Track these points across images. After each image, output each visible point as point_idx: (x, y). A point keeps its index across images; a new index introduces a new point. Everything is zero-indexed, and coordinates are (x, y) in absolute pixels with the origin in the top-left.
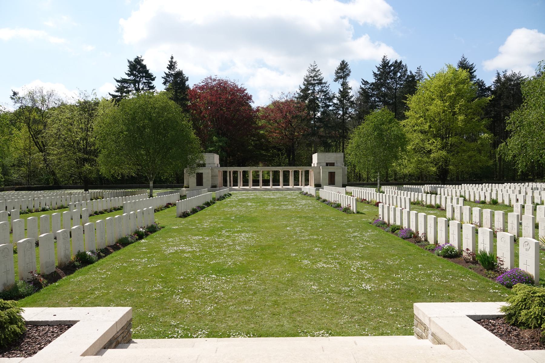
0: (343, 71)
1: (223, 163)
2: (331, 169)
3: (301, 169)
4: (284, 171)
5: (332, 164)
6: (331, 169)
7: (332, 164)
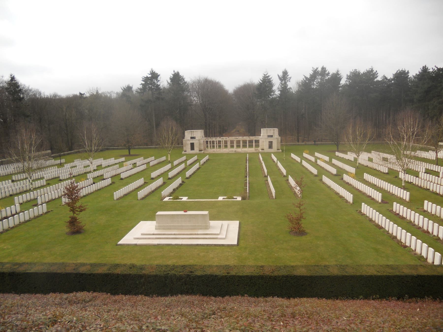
0: (284, 77)
1: (206, 135)
2: (270, 139)
3: (253, 138)
4: (255, 140)
5: (272, 136)
6: (192, 141)
7: (272, 136)
